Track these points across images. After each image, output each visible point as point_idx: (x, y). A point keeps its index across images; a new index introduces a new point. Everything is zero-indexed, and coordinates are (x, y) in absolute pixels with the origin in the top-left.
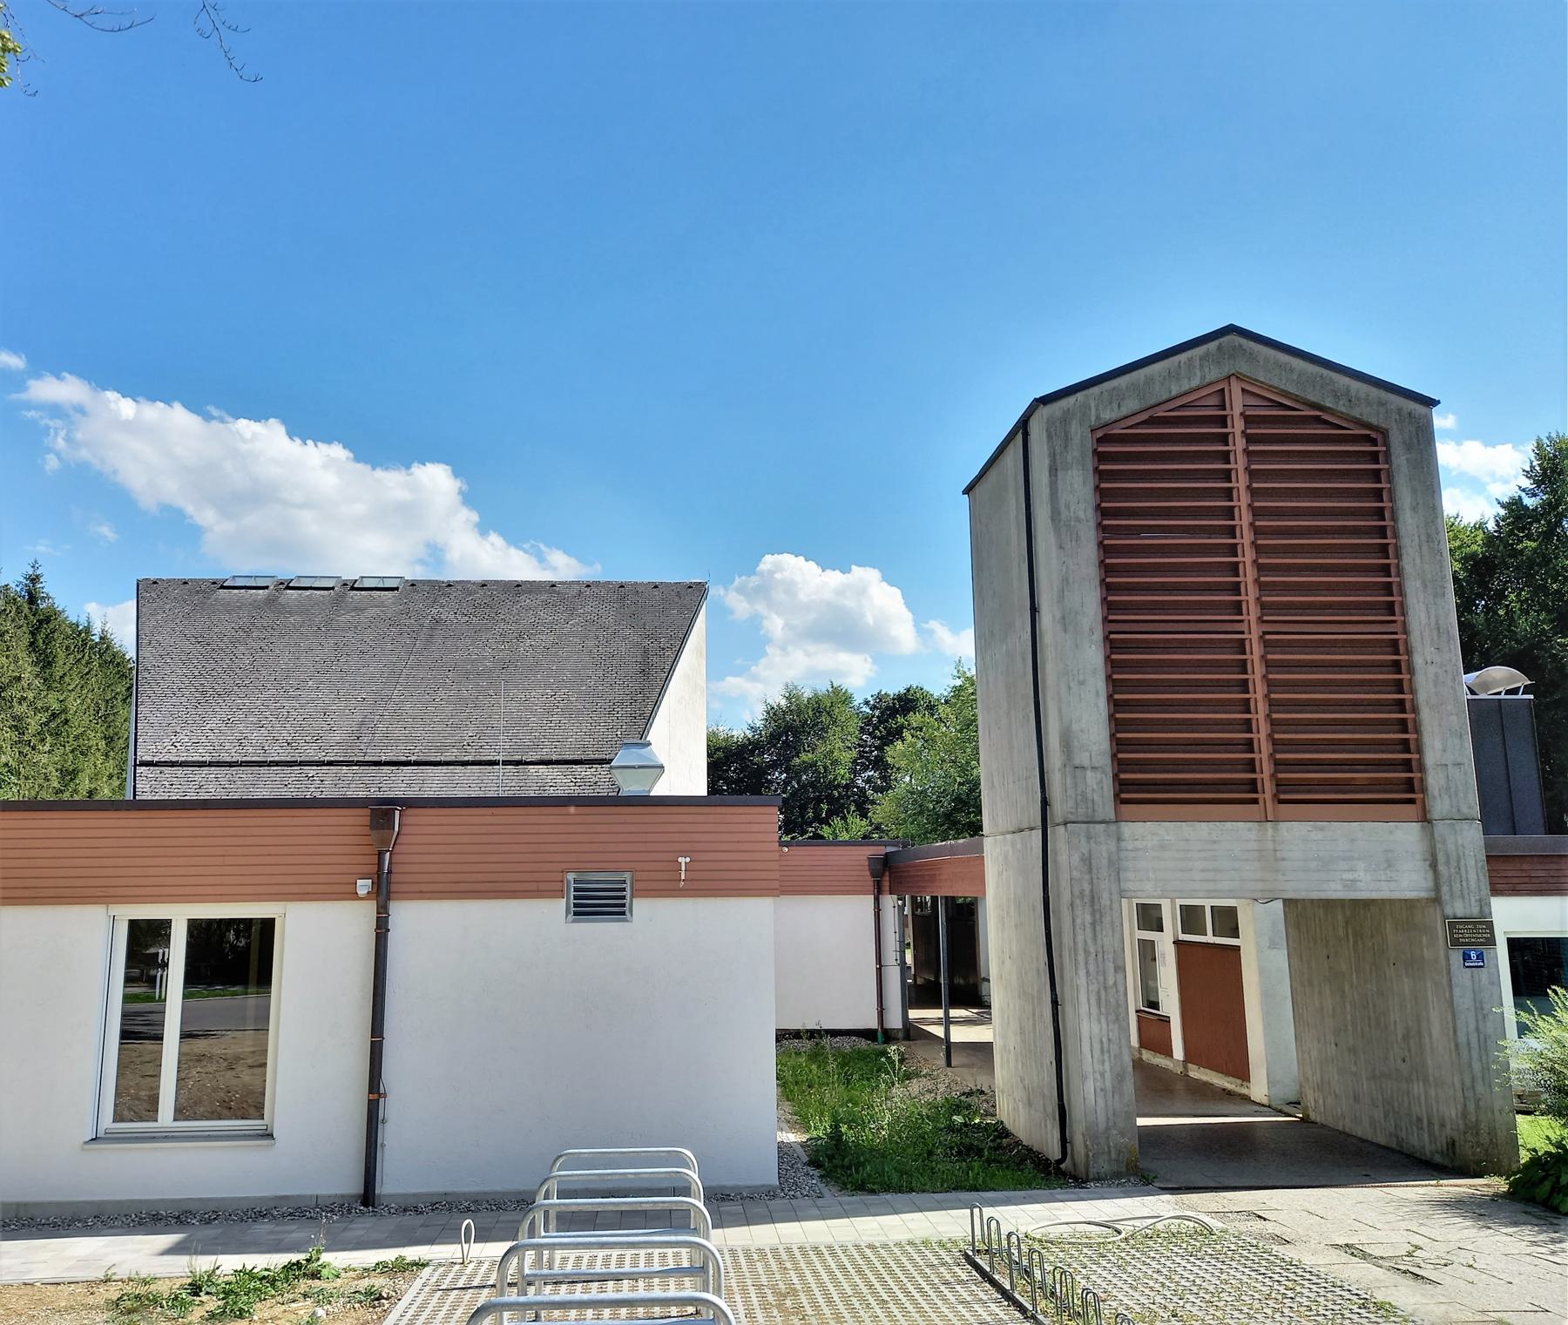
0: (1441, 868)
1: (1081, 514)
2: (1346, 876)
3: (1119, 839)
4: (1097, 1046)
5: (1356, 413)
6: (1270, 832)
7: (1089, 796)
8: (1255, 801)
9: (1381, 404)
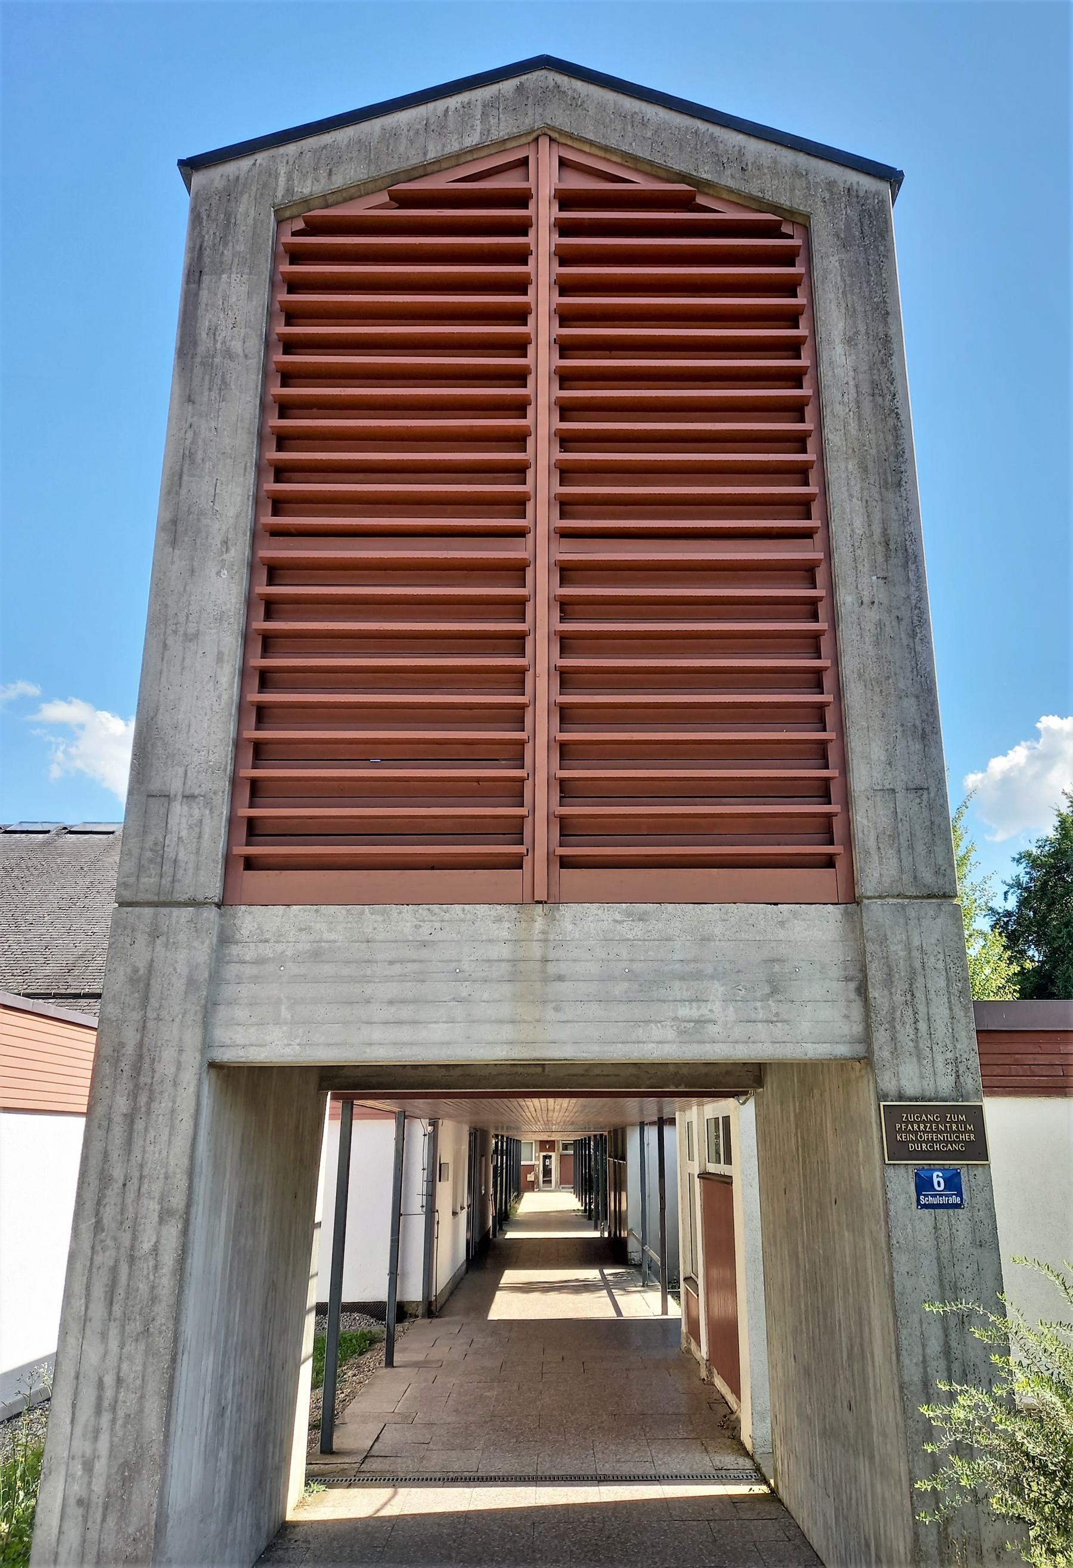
0: (875, 993)
1: (237, 346)
2: (684, 1011)
3: (225, 939)
4: (88, 1394)
5: (753, 188)
6: (539, 924)
7: (170, 853)
8: (516, 863)
9: (797, 173)
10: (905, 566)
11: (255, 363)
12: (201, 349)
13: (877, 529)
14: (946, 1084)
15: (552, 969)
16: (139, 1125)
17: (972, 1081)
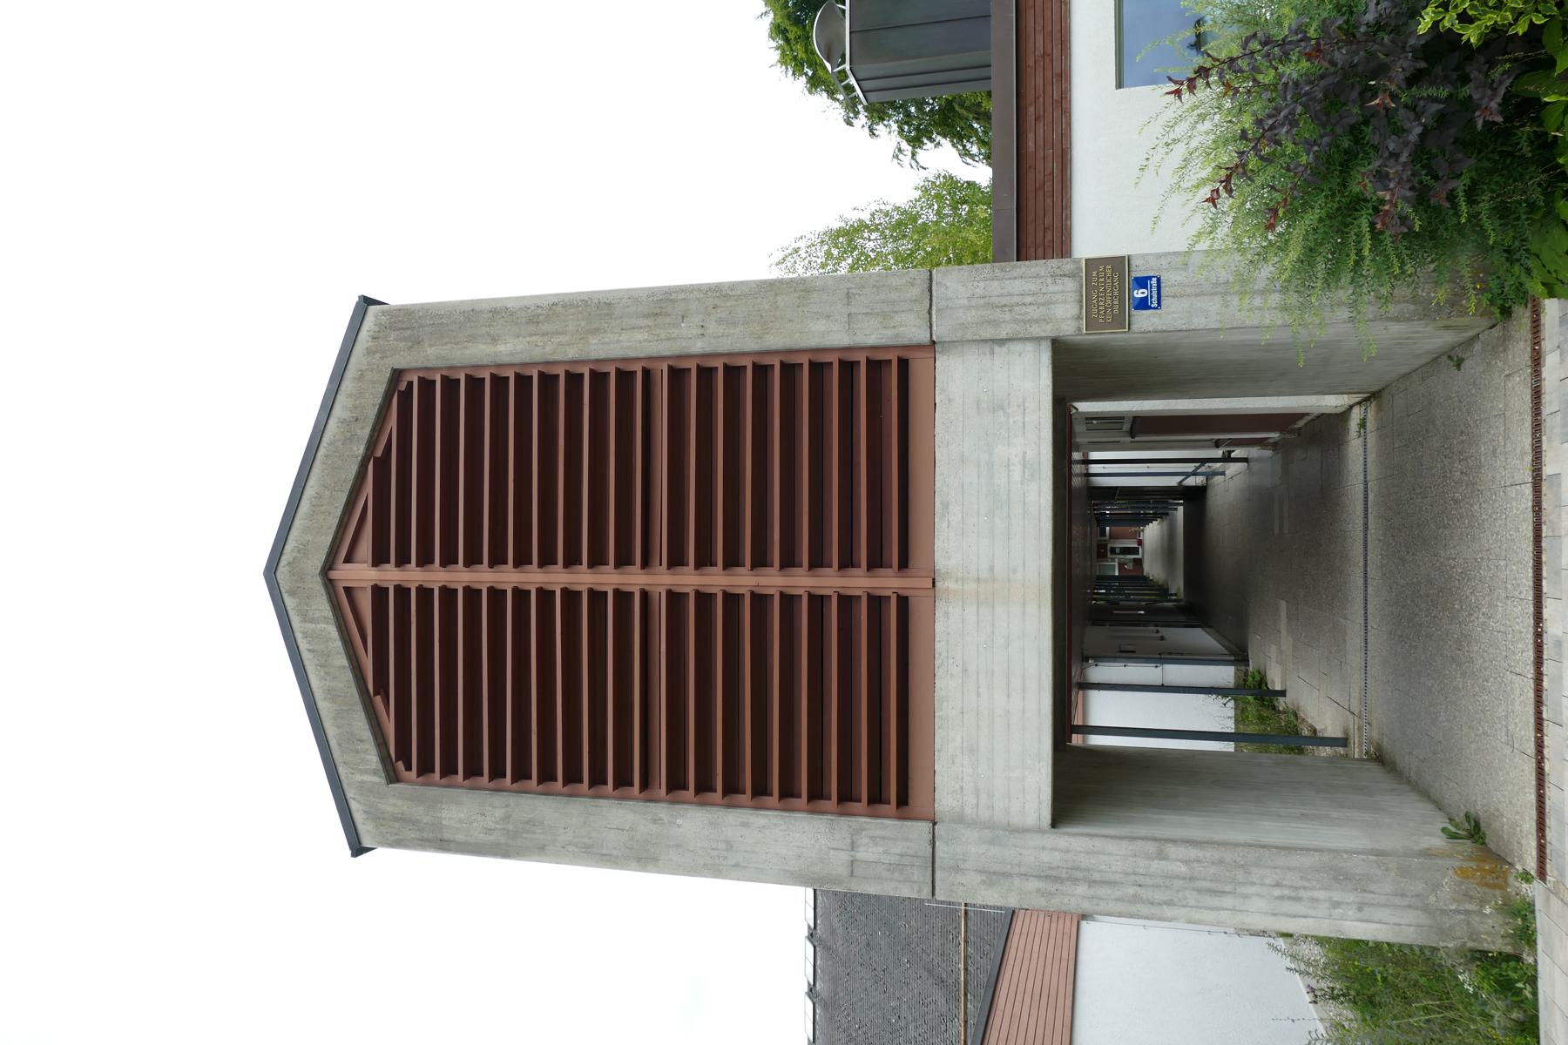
2: (1017, 475)
3: (960, 819)
4: (1287, 907)
6: (950, 584)
8: (903, 602)
9: (361, 377)
10: (673, 301)
11: (513, 799)
12: (502, 840)
13: (645, 322)
14: (1070, 285)
15: (984, 575)
16: (1097, 876)
17: (1067, 265)
